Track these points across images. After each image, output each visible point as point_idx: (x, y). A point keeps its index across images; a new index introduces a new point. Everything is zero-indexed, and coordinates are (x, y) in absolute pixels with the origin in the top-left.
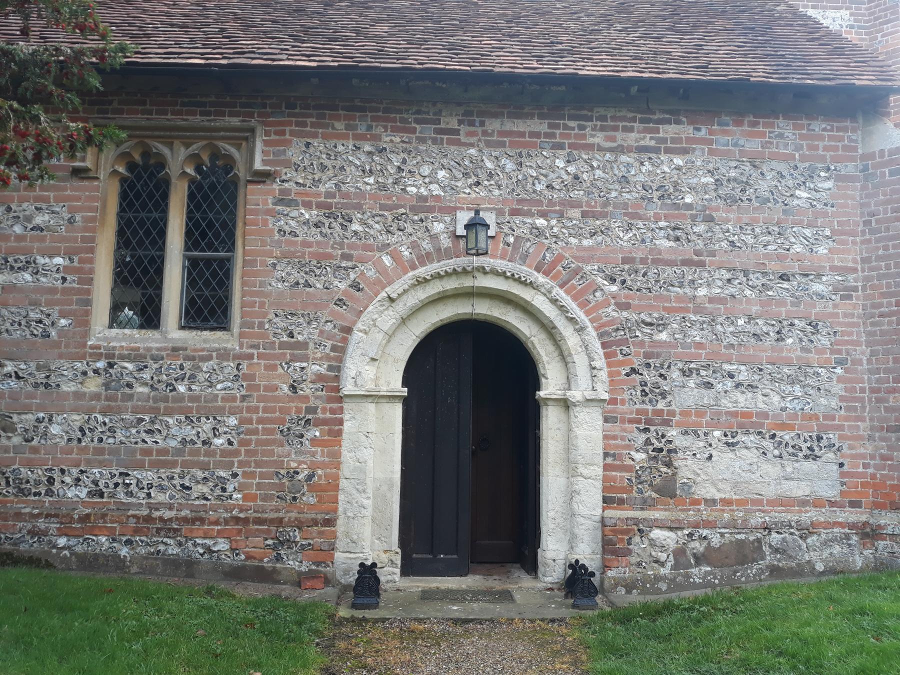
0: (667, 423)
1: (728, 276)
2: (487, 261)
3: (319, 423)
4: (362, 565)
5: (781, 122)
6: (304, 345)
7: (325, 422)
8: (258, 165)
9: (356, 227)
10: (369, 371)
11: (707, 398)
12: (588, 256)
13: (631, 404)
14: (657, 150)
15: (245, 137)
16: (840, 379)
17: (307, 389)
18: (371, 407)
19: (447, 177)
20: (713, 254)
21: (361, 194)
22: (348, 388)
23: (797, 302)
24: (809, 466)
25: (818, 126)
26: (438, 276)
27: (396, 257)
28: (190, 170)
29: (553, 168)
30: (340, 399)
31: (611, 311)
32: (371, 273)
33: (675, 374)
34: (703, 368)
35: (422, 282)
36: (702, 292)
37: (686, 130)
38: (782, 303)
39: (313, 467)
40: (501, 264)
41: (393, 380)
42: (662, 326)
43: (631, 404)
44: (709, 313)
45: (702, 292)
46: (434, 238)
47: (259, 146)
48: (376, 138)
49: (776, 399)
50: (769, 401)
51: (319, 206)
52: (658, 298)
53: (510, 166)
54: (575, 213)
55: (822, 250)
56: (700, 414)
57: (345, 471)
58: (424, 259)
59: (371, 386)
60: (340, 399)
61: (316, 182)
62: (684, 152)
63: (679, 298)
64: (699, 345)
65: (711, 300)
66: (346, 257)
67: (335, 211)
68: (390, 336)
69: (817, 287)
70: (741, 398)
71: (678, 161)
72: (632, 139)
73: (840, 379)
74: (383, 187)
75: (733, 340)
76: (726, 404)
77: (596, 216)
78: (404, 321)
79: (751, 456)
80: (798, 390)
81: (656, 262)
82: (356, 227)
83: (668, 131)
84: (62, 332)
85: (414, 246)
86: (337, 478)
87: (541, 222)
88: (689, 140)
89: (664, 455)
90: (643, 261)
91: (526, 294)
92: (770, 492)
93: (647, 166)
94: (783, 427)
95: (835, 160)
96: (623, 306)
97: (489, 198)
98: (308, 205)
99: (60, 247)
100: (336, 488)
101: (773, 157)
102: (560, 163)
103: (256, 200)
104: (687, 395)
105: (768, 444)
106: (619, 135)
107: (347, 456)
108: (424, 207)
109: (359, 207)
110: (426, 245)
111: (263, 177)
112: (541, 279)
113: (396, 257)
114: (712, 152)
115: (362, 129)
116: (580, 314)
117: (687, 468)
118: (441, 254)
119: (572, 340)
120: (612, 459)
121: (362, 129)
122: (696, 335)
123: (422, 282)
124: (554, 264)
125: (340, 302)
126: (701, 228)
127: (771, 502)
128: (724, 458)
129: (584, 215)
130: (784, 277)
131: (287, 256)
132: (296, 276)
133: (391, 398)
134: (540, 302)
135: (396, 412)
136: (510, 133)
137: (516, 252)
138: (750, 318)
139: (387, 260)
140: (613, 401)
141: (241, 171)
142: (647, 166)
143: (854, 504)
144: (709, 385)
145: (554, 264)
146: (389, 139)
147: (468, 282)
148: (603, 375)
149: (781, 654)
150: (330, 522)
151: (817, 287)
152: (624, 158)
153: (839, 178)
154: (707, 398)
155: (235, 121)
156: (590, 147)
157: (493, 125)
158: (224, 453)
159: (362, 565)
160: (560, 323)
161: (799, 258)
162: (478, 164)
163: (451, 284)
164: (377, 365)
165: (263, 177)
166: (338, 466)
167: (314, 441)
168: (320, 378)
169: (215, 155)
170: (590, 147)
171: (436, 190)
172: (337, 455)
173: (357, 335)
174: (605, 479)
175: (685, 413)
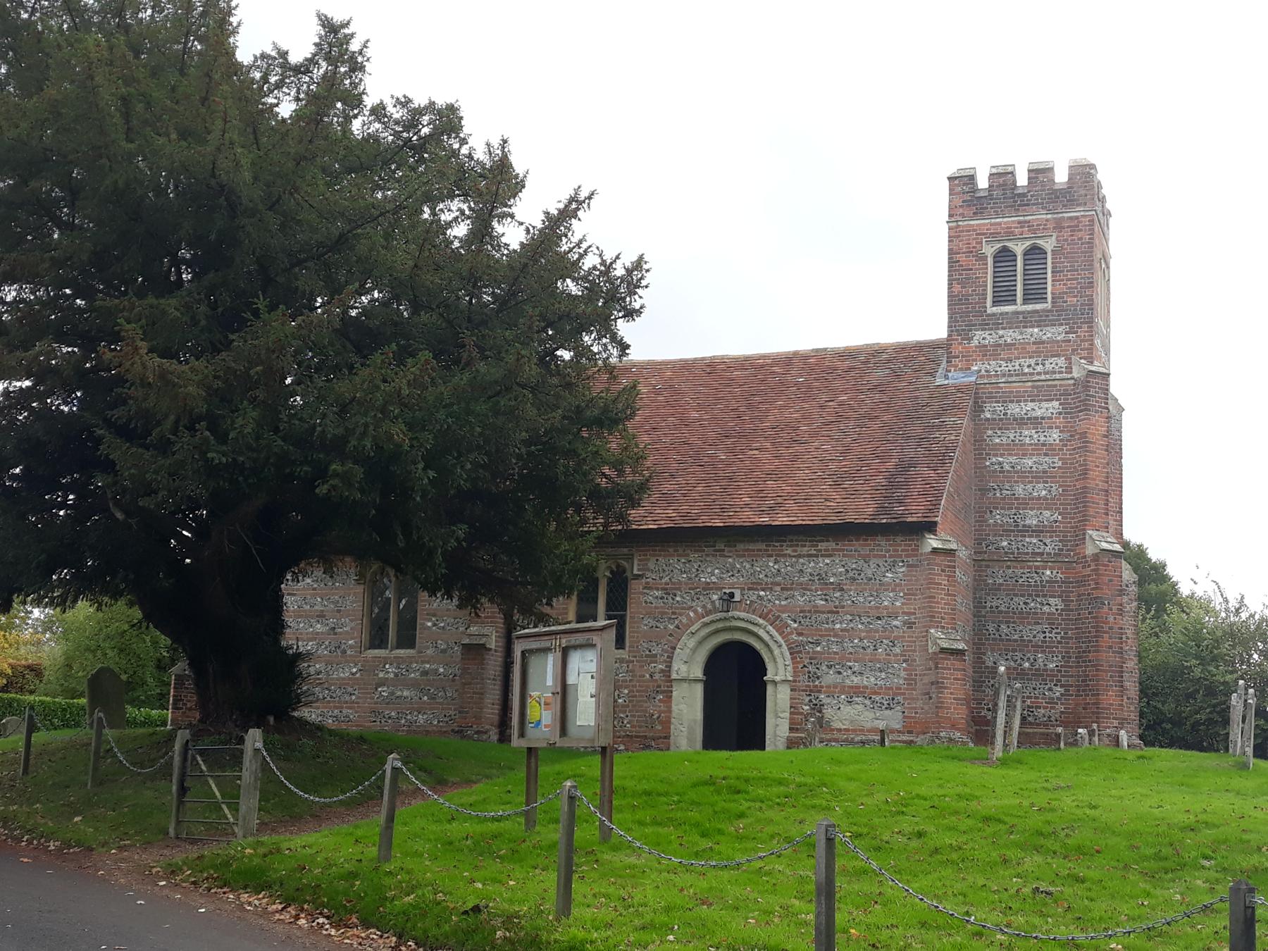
0: (819, 692)
1: (850, 618)
2: (736, 614)
3: (663, 692)
4: (962, 184)
5: (879, 538)
6: (655, 656)
7: (663, 692)
8: (635, 572)
9: (678, 598)
10: (684, 668)
11: (839, 679)
12: (784, 609)
13: (803, 681)
14: (817, 556)
15: (630, 558)
16: (905, 670)
17: (657, 676)
18: (685, 685)
19: (715, 571)
20: (843, 607)
21: (680, 583)
22: (674, 676)
23: (885, 630)
24: (888, 712)
25: (899, 539)
26: (712, 622)
27: (695, 612)
28: (608, 574)
29: (767, 566)
30: (671, 681)
31: (794, 637)
32: (684, 621)
33: (824, 668)
34: (839, 663)
35: (706, 625)
36: (838, 626)
37: (831, 545)
38: (877, 631)
39: (660, 712)
40: (743, 615)
41: (698, 672)
42: (818, 644)
43: (803, 681)
44: (840, 636)
45: (838, 626)
46: (713, 602)
47: (636, 562)
48: (688, 555)
49: (873, 679)
50: (869, 680)
51: (663, 589)
52: (817, 630)
53: (748, 566)
54: (778, 588)
55: (898, 604)
56: (835, 687)
57: (674, 715)
58: (708, 613)
59: (685, 675)
60: (671, 681)
61: (661, 578)
62: (830, 556)
63: (826, 630)
64: (836, 653)
65: (842, 630)
66: (674, 613)
67: (669, 591)
68: (694, 650)
69: (895, 623)
70: (855, 680)
71: (827, 561)
72: (805, 550)
73: (905, 670)
74: (690, 579)
75: (851, 650)
76: (848, 682)
77: (787, 589)
78: (700, 643)
79: (860, 707)
80: (883, 675)
81: (816, 612)
82: (678, 598)
83: (822, 546)
84: (430, 620)
85: (704, 607)
86: (670, 718)
87: (762, 593)
88: (834, 550)
89: (818, 708)
90: (810, 611)
91: (755, 629)
92: (869, 725)
93: (812, 564)
94: (876, 693)
95: (907, 556)
96: (800, 634)
97: (734, 583)
98: (657, 589)
99: (1026, 301)
100: (669, 722)
101: (875, 556)
102: (771, 564)
103: (635, 587)
104: (830, 678)
105: (868, 702)
106: (799, 549)
107: (674, 707)
108: (708, 587)
109: (679, 589)
110: (709, 606)
111: (637, 577)
112: (761, 621)
113: (695, 612)
114: (844, 556)
115: (681, 552)
116: (779, 638)
117: (828, 712)
118: (715, 610)
119: (776, 652)
120: (793, 708)
121: (681, 552)
122: (835, 648)
123: (706, 625)
124: (767, 614)
125: (671, 635)
126: (837, 594)
127: (869, 731)
128: (847, 710)
129: (782, 589)
130: (879, 618)
131: (649, 614)
132: (653, 623)
133: (696, 681)
134: (761, 633)
135: (699, 690)
136: (748, 550)
137: (751, 608)
138: (861, 640)
139: (692, 614)
140: (795, 681)
141: (628, 574)
142: (812, 564)
143: (910, 732)
144: (840, 673)
145: (767, 614)
146: (694, 556)
147: (728, 624)
148: (789, 668)
149: (1139, 917)
150: (667, 737)
151: (895, 623)
152: (801, 560)
153: (909, 566)
154: (839, 679)
155: (625, 550)
156: (785, 555)
157: (741, 546)
158: (623, 706)
159: (962, 184)
160: (771, 643)
161: (886, 608)
162: (733, 567)
163: (720, 625)
164: (689, 664)
165: (637, 577)
166: (670, 712)
167: (660, 701)
168: (662, 671)
169: (618, 566)
170: (785, 555)
171: (714, 579)
172: (670, 707)
173: (678, 650)
174: (791, 719)
175: (828, 687)
